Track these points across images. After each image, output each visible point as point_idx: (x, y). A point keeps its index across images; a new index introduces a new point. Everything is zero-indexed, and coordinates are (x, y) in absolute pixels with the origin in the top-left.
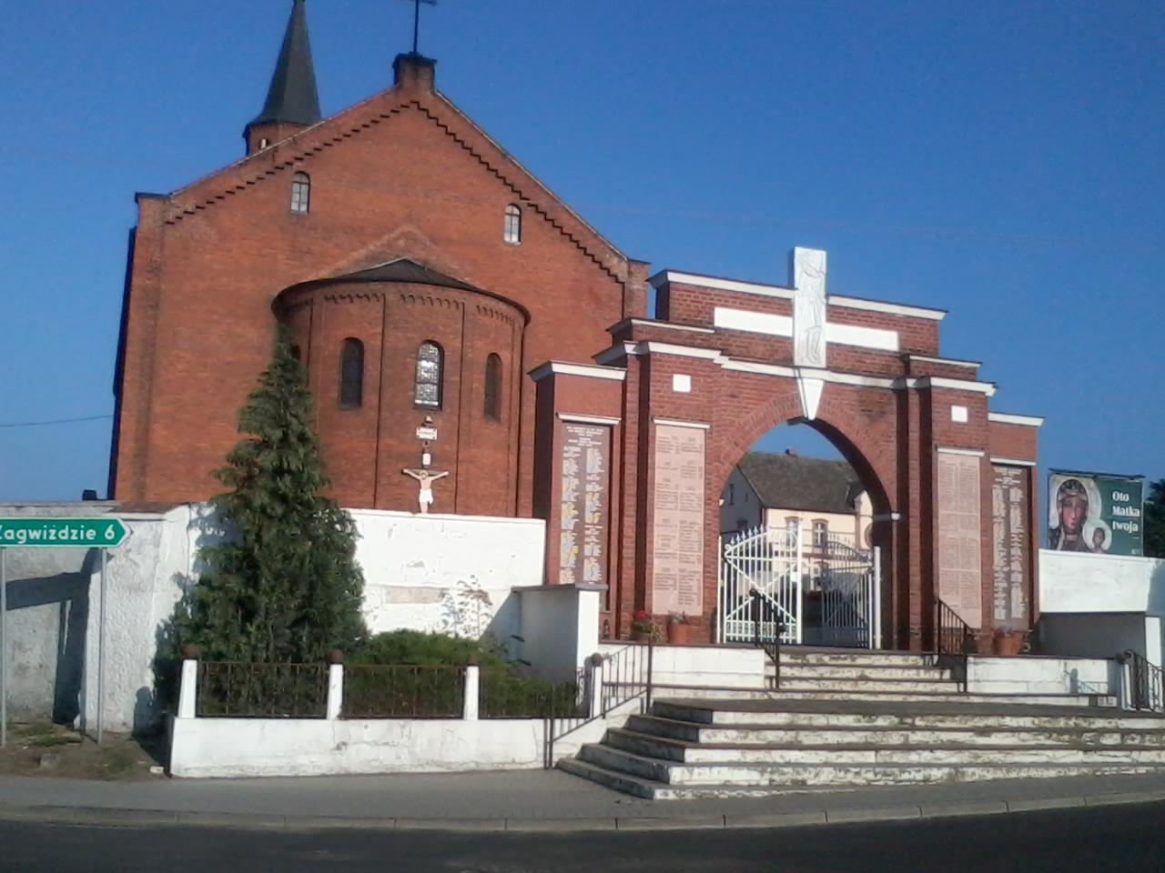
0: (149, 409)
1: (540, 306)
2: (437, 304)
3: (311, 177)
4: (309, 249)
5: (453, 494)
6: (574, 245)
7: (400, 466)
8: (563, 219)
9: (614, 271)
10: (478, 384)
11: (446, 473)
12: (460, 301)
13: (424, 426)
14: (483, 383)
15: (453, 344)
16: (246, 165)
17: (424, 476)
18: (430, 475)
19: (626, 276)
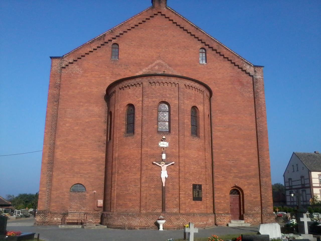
0: (54, 143)
1: (217, 89)
2: (166, 85)
3: (119, 45)
4: (119, 74)
5: (178, 173)
6: (230, 62)
7: (152, 160)
8: (224, 51)
9: (248, 71)
10: (188, 120)
11: (173, 163)
12: (176, 83)
13: (162, 141)
14: (190, 119)
15: (174, 102)
16: (93, 42)
17: (163, 165)
18: (166, 164)
19: (253, 73)
